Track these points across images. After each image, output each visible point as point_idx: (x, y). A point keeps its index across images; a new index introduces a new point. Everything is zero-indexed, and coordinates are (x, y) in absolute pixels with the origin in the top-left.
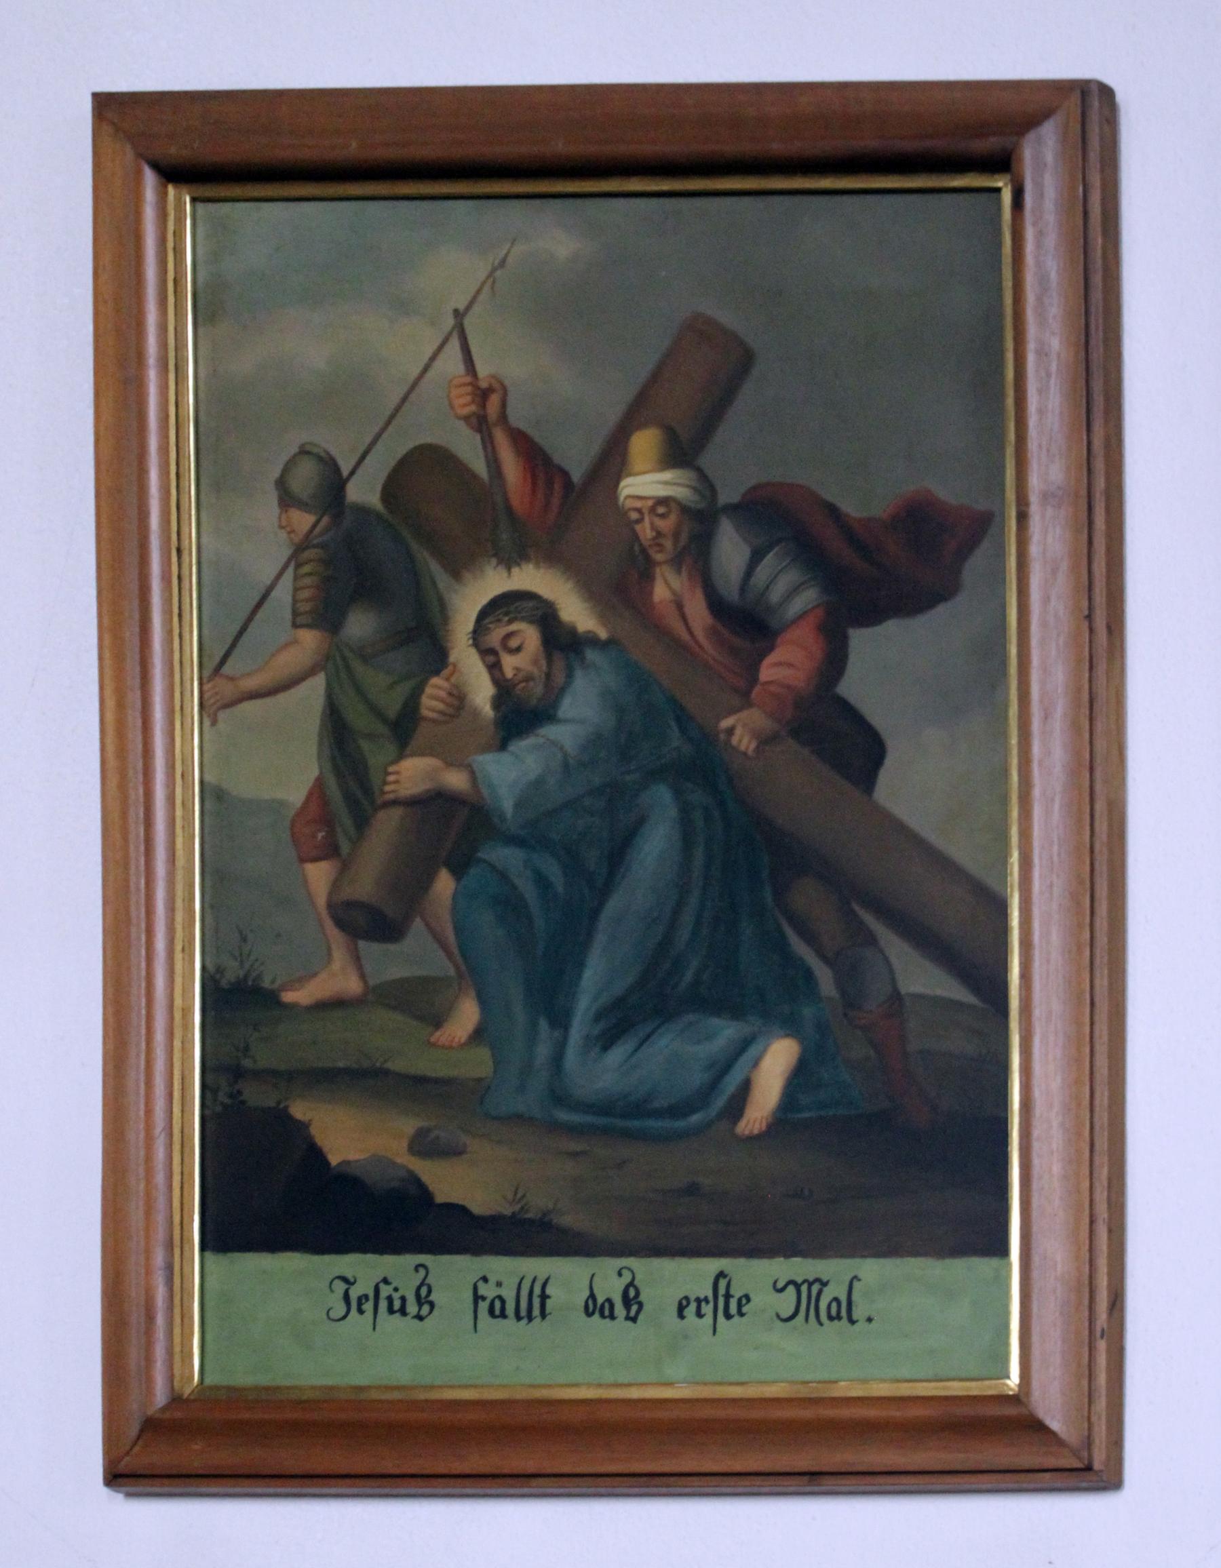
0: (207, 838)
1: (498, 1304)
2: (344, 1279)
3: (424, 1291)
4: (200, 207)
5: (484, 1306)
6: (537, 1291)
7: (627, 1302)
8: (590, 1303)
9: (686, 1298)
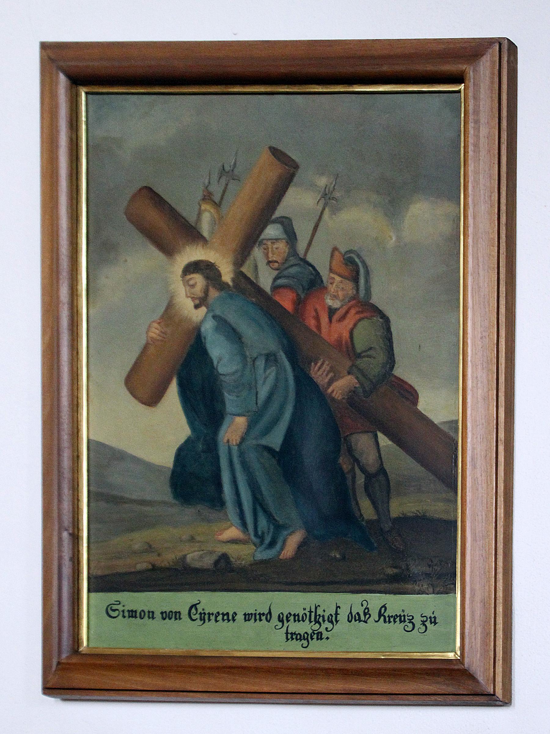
0: (92, 470)
4: (90, 97)
7: (365, 614)
8: (269, 616)
9: (218, 613)
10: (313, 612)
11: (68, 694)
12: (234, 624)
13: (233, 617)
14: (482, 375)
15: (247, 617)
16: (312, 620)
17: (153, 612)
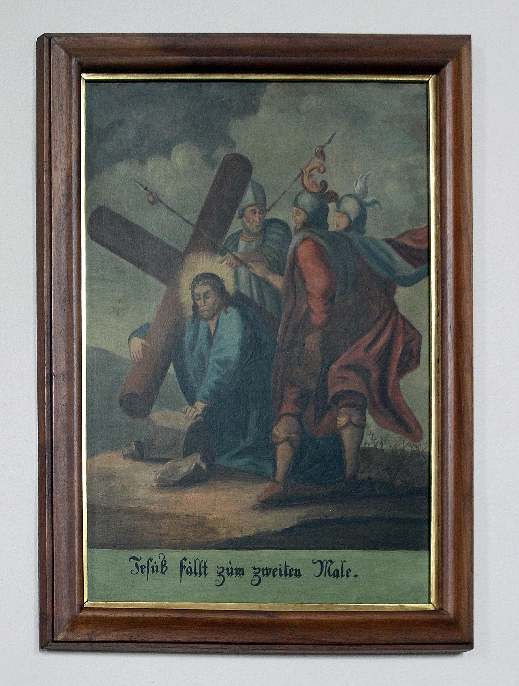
1: (189, 569)
2: (134, 558)
3: (164, 563)
5: (184, 571)
6: (203, 565)
7: (162, 567)
10: (203, 567)
12: (280, 579)
13: (348, 573)
14: (47, 254)
16: (287, 574)
17: (243, 569)
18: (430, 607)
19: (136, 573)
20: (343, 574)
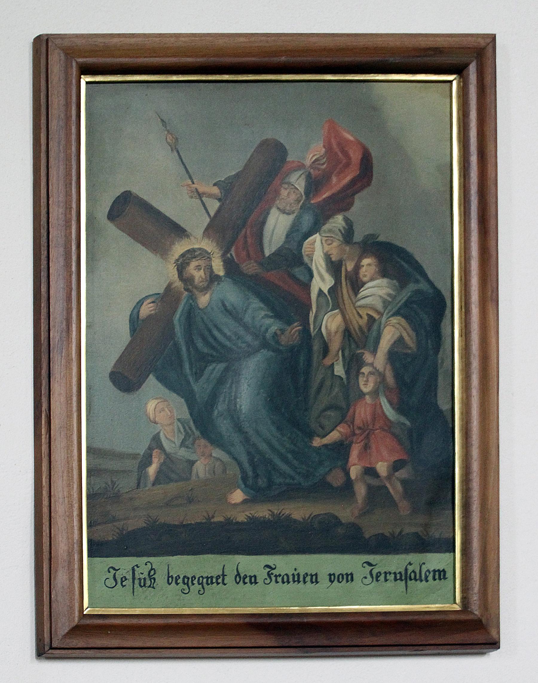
1: (285, 577)
2: (370, 564)
9: (307, 574)
11: (402, 650)
15: (170, 579)
16: (290, 581)
17: (255, 577)
18: (457, 607)
19: (109, 586)
20: (305, 580)
